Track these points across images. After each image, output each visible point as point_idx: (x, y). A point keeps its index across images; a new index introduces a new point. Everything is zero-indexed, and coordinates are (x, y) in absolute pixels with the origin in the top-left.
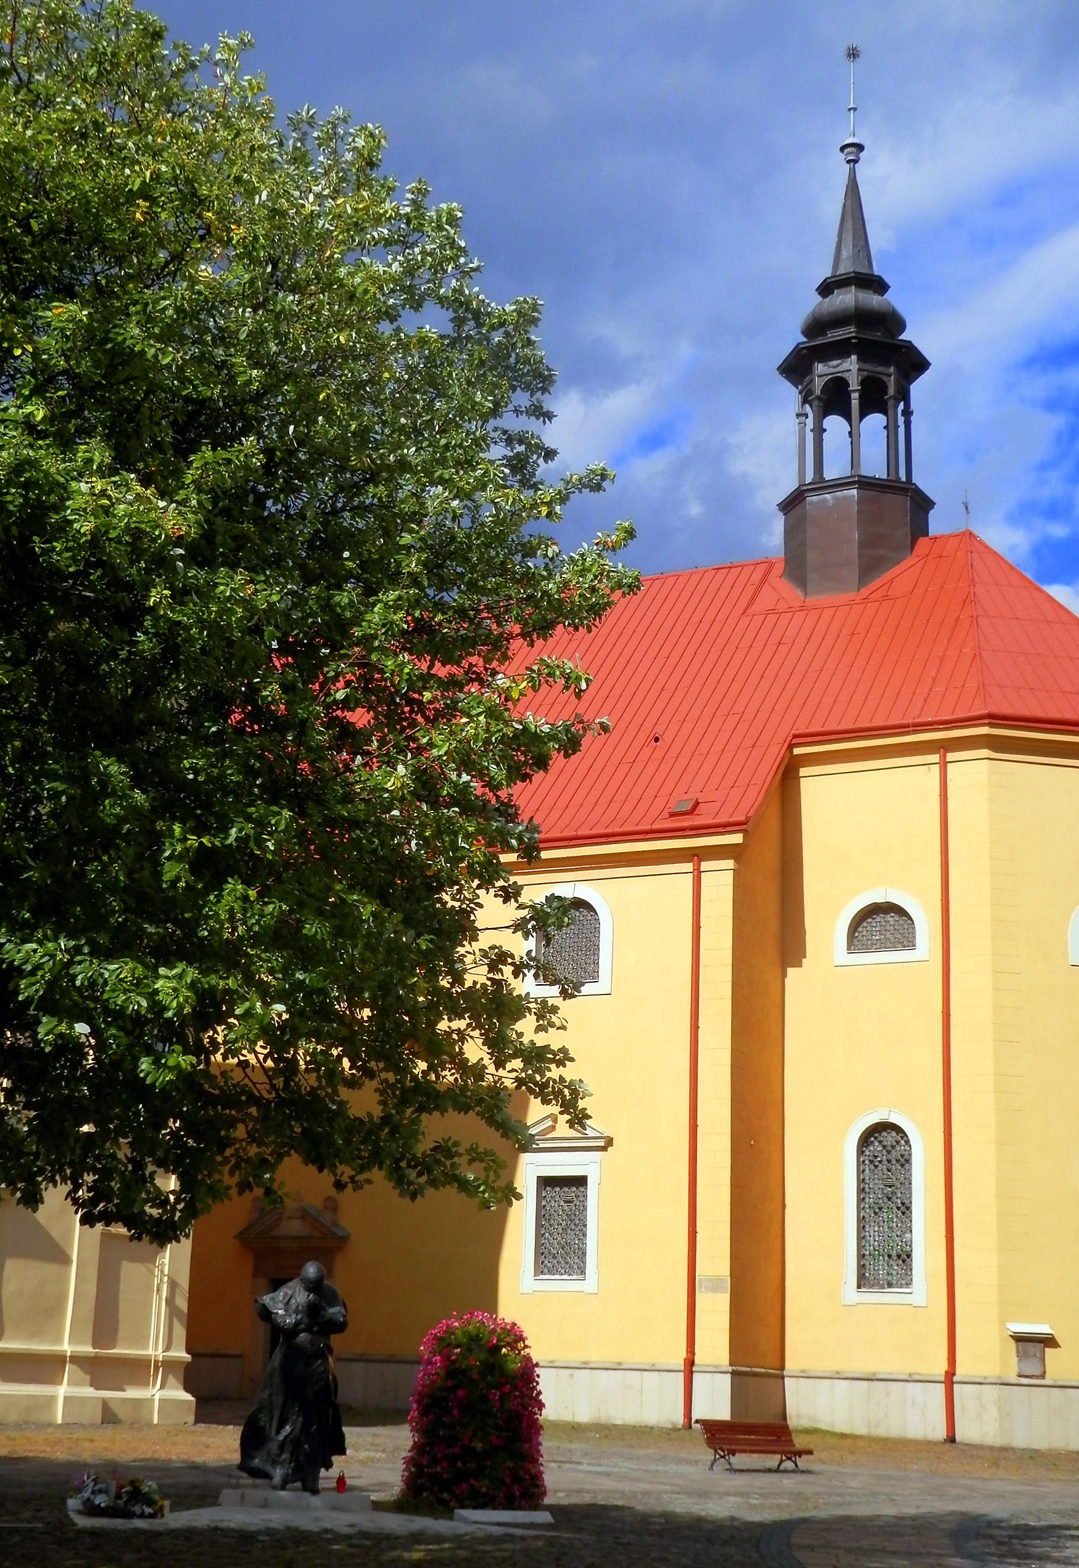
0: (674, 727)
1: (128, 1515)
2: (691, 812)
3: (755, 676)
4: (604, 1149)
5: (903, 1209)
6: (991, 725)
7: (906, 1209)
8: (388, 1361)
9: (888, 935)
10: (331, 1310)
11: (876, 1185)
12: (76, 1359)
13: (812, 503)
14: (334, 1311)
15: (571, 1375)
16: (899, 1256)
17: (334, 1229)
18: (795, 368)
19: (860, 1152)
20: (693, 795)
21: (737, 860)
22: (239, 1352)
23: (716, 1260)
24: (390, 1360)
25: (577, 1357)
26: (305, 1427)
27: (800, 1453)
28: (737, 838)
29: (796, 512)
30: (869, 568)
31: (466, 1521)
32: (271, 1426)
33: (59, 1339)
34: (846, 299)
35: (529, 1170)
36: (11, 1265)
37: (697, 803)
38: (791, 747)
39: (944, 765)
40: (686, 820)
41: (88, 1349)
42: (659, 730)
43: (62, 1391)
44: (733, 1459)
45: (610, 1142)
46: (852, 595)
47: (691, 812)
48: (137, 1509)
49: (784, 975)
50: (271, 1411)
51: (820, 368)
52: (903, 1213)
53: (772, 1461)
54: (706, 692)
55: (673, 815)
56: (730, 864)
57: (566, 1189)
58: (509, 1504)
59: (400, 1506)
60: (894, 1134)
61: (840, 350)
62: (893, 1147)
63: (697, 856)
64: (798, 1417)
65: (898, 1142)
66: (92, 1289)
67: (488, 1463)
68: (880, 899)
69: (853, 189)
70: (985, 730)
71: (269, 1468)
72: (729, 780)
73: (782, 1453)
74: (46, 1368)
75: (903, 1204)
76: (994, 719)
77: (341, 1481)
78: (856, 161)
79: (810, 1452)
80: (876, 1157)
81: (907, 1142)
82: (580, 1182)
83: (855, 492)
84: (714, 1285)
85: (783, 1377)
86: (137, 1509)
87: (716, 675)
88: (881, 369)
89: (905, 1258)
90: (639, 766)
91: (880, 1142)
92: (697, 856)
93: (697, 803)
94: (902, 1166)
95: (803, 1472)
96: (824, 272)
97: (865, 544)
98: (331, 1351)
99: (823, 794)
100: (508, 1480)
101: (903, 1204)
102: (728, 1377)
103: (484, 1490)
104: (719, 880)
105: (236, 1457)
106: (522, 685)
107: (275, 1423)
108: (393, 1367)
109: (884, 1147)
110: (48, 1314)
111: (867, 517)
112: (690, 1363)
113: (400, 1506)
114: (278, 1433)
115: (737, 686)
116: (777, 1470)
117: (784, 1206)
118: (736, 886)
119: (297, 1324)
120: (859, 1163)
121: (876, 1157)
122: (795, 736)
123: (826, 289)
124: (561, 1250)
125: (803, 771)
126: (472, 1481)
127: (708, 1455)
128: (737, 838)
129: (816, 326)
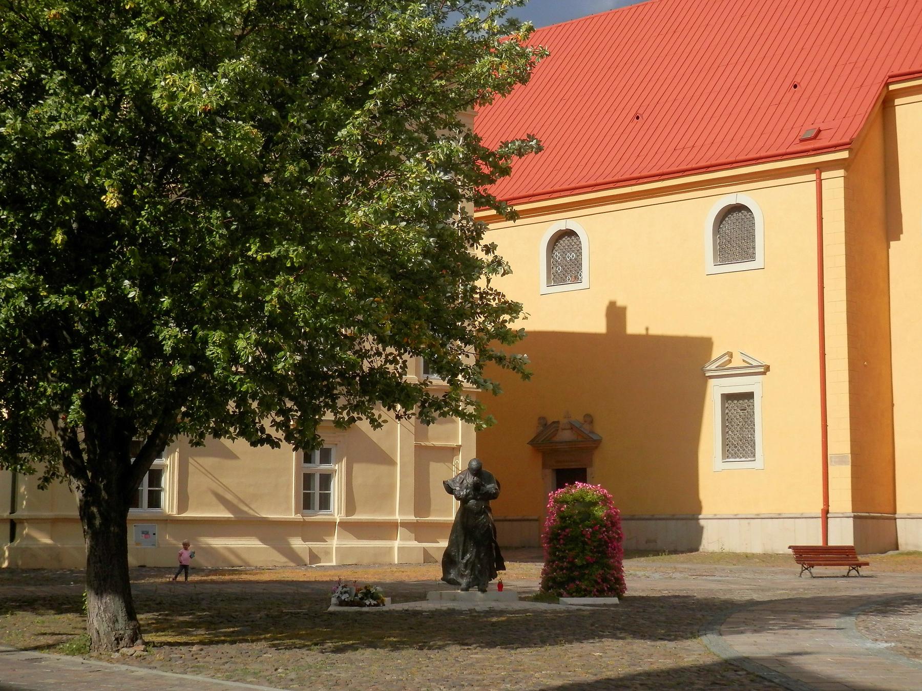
0: (807, 77)
1: (360, 604)
2: (815, 137)
3: (867, 34)
4: (764, 373)
10: (488, 486)
12: (405, 525)
14: (491, 487)
17: (591, 435)
20: (816, 126)
21: (846, 169)
22: (536, 517)
23: (841, 442)
24: (673, 518)
25: (752, 511)
26: (477, 555)
27: (860, 565)
28: (844, 155)
31: (566, 604)
33: (392, 512)
35: (716, 390)
37: (819, 131)
38: (887, 85)
40: (812, 144)
41: (412, 518)
42: (798, 80)
43: (397, 544)
44: (813, 570)
45: (767, 368)
47: (815, 137)
48: (367, 602)
49: (888, 247)
50: (458, 546)
53: (844, 570)
54: (833, 47)
55: (802, 141)
56: (841, 172)
58: (601, 593)
59: (537, 598)
63: (818, 168)
64: (907, 544)
66: (411, 480)
67: (587, 572)
71: (460, 580)
72: (842, 114)
73: (849, 565)
74: (386, 530)
77: (500, 586)
79: (867, 564)
82: (750, 396)
84: (840, 460)
85: (895, 519)
86: (367, 602)
87: (840, 35)
90: (782, 106)
92: (818, 168)
93: (819, 131)
95: (863, 577)
98: (490, 510)
100: (600, 581)
102: (851, 521)
103: (583, 587)
104: (835, 182)
105: (441, 575)
106: (492, 124)
107: (461, 553)
108: (633, 523)
110: (384, 497)
112: (826, 512)
113: (537, 598)
114: (463, 559)
115: (854, 42)
116: (848, 576)
117: (893, 405)
118: (847, 188)
119: (467, 495)
122: (890, 77)
124: (739, 442)
125: (897, 101)
127: (798, 568)
128: (844, 155)
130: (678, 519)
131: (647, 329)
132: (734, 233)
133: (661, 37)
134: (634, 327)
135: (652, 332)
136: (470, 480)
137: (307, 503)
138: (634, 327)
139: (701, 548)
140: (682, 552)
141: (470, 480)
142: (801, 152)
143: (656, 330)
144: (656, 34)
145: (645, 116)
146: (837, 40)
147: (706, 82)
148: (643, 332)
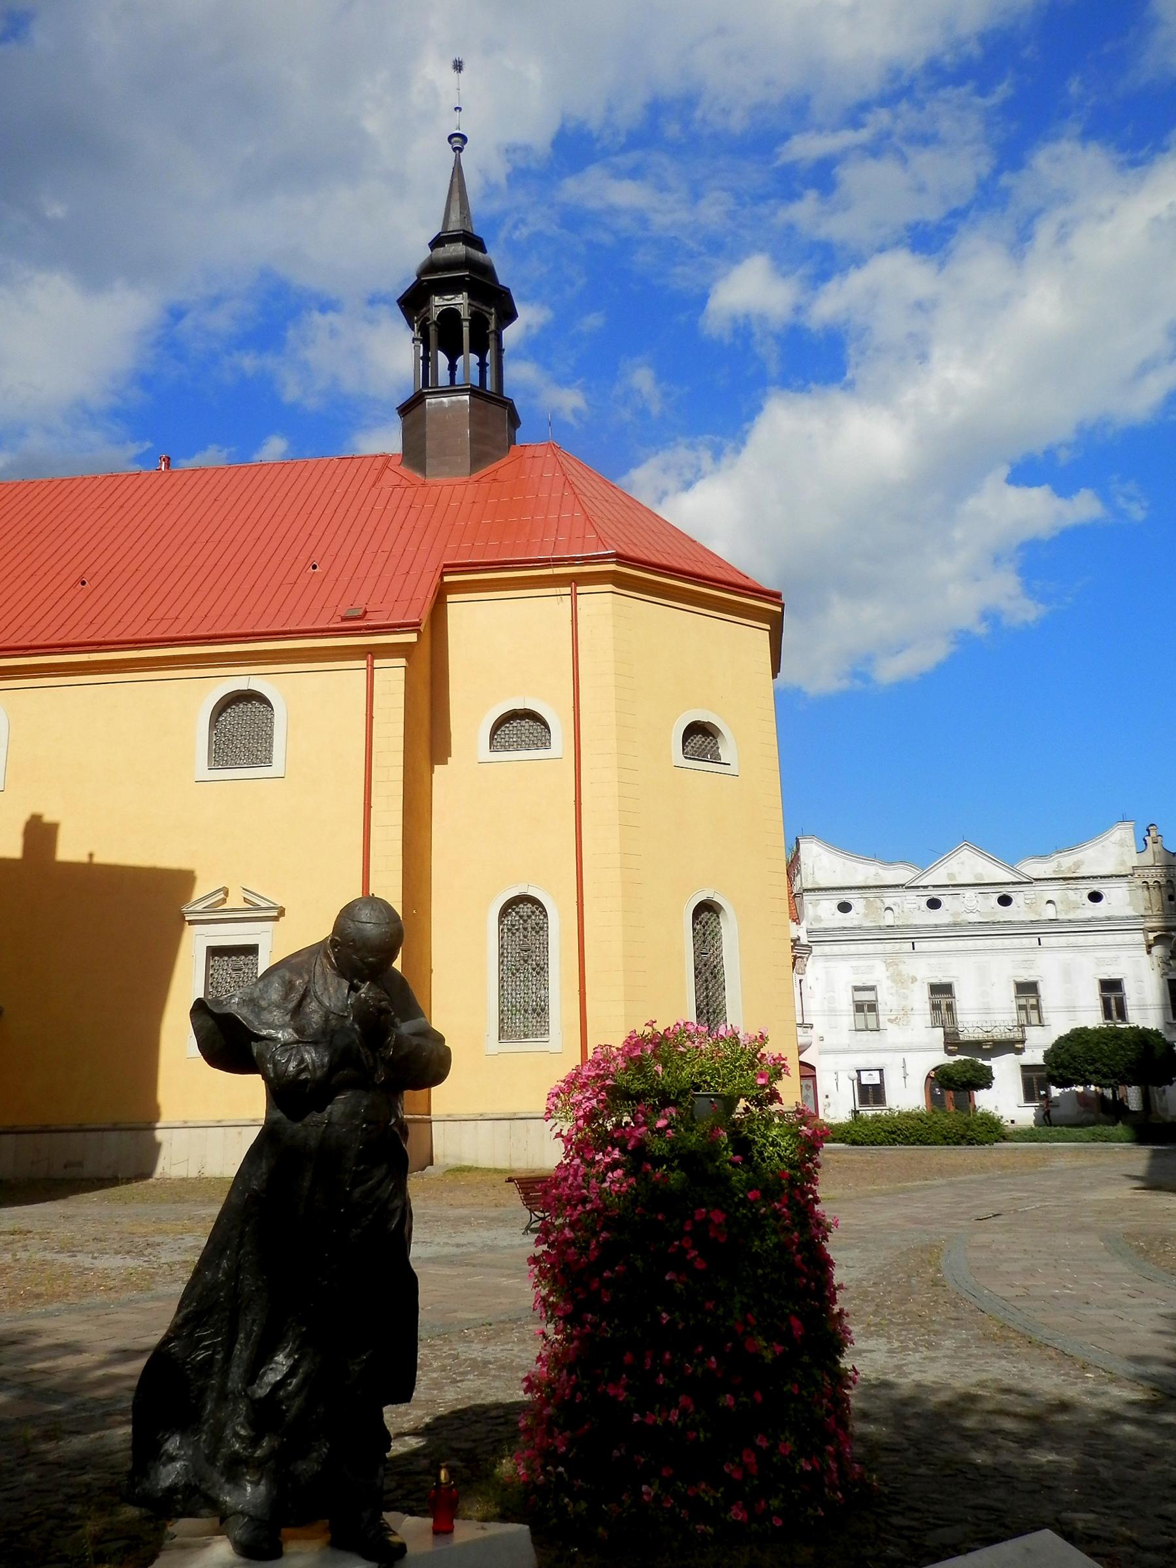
3: (395, 526)
4: (276, 919)
5: (538, 969)
6: (618, 563)
7: (541, 969)
8: (41, 1132)
9: (524, 738)
11: (513, 950)
13: (430, 404)
15: (240, 1133)
16: (534, 1010)
18: (413, 302)
19: (501, 922)
24: (44, 1130)
28: (412, 638)
29: (416, 412)
30: (478, 460)
32: (228, 1359)
34: (458, 250)
36: (385, 1409)
37: (366, 612)
39: (371, 671)
45: (282, 912)
46: (466, 478)
49: (432, 771)
51: (437, 300)
52: (538, 973)
56: (402, 662)
57: (234, 958)
60: (529, 905)
61: (451, 287)
62: (529, 917)
63: (371, 653)
65: (533, 913)
68: (519, 706)
69: (458, 170)
70: (613, 567)
75: (538, 965)
76: (621, 559)
78: (461, 150)
80: (514, 926)
81: (546, 916)
83: (467, 398)
88: (484, 308)
89: (541, 1011)
91: (517, 913)
93: (366, 612)
94: (537, 932)
96: (435, 230)
97: (474, 439)
99: (468, 618)
101: (538, 965)
109: (521, 917)
111: (476, 420)
120: (501, 931)
121: (514, 926)
122: (446, 566)
123: (437, 243)
125: (450, 598)
126: (762, 1442)
128: (412, 638)
129: (431, 267)
130: (122, 1130)
131: (91, 855)
132: (240, 730)
133: (101, 511)
134: (68, 850)
135: (99, 859)
136: (332, 995)
137: (1107, 1014)
138: (68, 850)
139: (158, 1172)
140: (128, 1181)
141: (332, 995)
142: (351, 634)
143: (108, 855)
144: (95, 505)
145: (95, 582)
146: (356, 530)
147: (114, 605)
148: (84, 859)
